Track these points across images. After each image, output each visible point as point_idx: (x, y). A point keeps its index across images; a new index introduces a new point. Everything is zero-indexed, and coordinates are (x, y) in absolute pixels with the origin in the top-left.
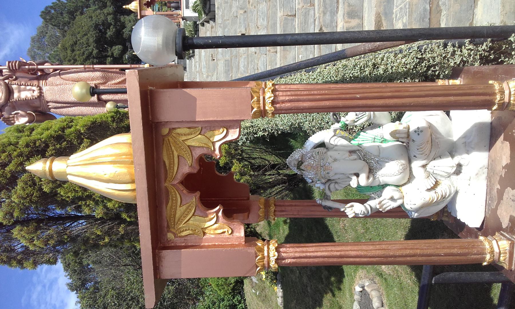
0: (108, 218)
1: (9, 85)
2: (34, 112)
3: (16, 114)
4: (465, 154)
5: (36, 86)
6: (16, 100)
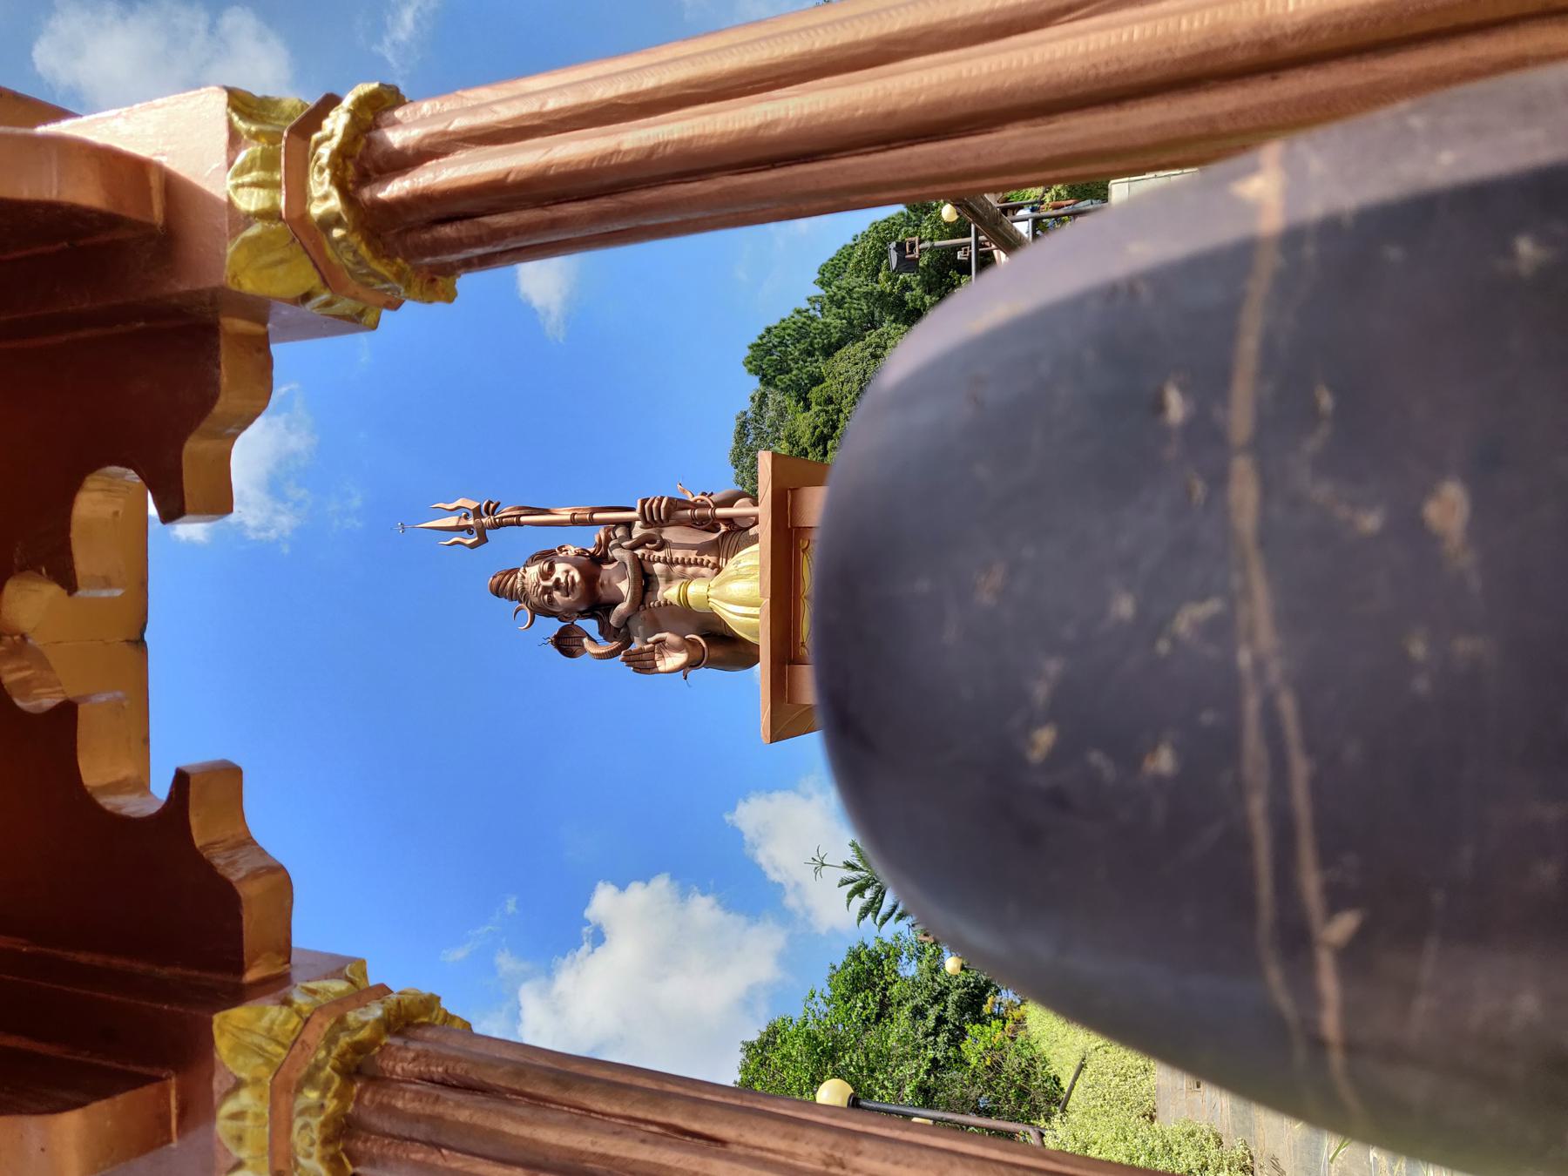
1: (645, 563)
2: (702, 637)
3: (657, 642)
5: (710, 565)
6: (659, 603)
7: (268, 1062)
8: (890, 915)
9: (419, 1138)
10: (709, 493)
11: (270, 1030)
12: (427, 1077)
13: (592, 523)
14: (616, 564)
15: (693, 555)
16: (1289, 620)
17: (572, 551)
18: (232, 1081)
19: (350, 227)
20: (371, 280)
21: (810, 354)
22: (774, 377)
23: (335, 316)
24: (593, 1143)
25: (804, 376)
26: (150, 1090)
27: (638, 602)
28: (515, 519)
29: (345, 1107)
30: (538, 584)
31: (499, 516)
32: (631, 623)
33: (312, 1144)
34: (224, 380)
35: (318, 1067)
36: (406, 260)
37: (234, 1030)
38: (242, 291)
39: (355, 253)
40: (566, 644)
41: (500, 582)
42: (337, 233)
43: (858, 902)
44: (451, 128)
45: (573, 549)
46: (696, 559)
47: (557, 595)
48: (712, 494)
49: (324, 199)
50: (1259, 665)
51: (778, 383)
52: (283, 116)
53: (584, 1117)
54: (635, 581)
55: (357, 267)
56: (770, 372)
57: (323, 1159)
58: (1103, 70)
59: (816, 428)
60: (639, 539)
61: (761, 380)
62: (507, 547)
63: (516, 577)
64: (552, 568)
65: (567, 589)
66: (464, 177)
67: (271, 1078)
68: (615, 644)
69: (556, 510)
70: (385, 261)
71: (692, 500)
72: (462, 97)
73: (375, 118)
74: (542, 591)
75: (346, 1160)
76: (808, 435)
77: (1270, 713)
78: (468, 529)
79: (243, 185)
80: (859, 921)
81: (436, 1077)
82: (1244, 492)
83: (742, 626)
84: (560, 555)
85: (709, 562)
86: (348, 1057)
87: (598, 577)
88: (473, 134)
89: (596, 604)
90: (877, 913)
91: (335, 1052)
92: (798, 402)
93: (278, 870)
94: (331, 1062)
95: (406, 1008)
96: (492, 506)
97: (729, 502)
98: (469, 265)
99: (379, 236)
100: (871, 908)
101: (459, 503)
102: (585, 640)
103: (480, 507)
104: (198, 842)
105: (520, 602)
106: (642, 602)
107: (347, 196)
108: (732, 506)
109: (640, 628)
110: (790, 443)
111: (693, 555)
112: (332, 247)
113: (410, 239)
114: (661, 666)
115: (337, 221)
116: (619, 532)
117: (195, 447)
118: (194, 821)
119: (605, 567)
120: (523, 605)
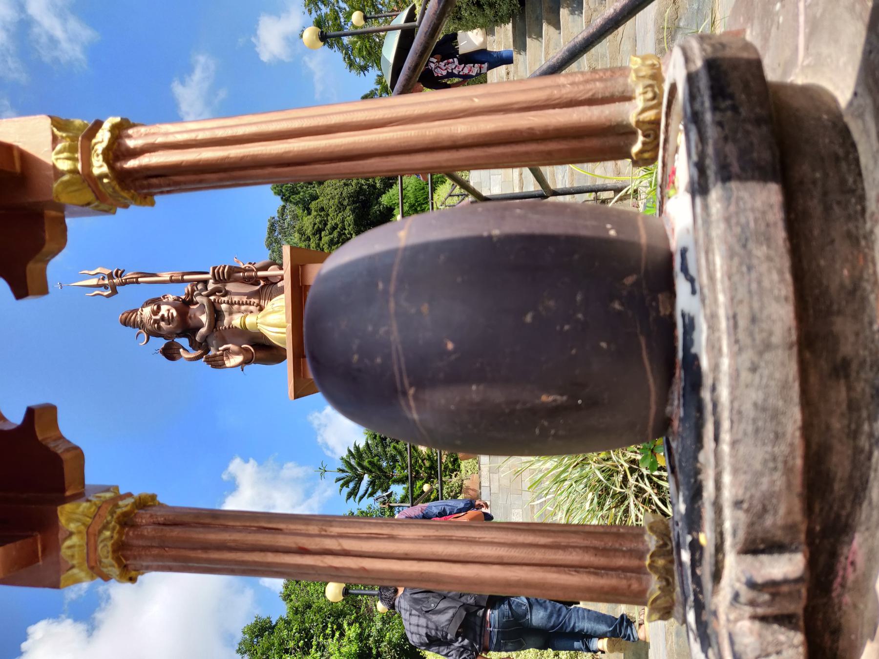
0: (127, 529)
1: (216, 304)
2: (252, 346)
4: (126, 582)
7: (84, 524)
8: (364, 495)
10: (253, 263)
11: (83, 512)
13: (183, 281)
14: (198, 305)
15: (244, 299)
17: (171, 298)
18: (68, 533)
20: (120, 199)
22: (290, 197)
25: (307, 195)
26: (30, 540)
27: (212, 326)
28: (135, 280)
30: (151, 318)
31: (124, 278)
32: (209, 340)
33: (108, 552)
34: (47, 237)
35: (108, 523)
36: (135, 191)
39: (113, 188)
40: (170, 353)
41: (126, 318)
42: (105, 181)
43: (346, 490)
45: (172, 297)
46: (247, 301)
47: (162, 324)
48: (255, 263)
49: (99, 167)
51: (292, 200)
53: (226, 528)
56: (287, 194)
57: (113, 558)
58: (403, 145)
59: (315, 224)
60: (212, 290)
61: (282, 198)
62: (128, 297)
63: (137, 314)
64: (159, 308)
65: (169, 320)
68: (199, 352)
69: (158, 274)
71: (243, 267)
74: (153, 322)
76: (310, 228)
77: (397, 351)
78: (105, 287)
79: (60, 159)
80: (347, 500)
81: (161, 522)
82: (392, 305)
83: (276, 339)
84: (164, 301)
85: (254, 302)
87: (188, 313)
89: (187, 328)
90: (356, 495)
91: (115, 516)
92: (304, 210)
93: (77, 448)
94: (114, 520)
96: (119, 272)
97: (265, 268)
98: (162, 193)
100: (353, 493)
101: (98, 270)
102: (181, 350)
103: (112, 272)
104: (40, 438)
105: (140, 329)
106: (215, 327)
107: (111, 166)
108: (267, 270)
109: (214, 342)
110: (300, 234)
111: (244, 299)
113: (137, 183)
114: (228, 363)
115: (106, 176)
116: (200, 287)
117: (32, 267)
118: (37, 429)
119: (192, 307)
120: (142, 331)
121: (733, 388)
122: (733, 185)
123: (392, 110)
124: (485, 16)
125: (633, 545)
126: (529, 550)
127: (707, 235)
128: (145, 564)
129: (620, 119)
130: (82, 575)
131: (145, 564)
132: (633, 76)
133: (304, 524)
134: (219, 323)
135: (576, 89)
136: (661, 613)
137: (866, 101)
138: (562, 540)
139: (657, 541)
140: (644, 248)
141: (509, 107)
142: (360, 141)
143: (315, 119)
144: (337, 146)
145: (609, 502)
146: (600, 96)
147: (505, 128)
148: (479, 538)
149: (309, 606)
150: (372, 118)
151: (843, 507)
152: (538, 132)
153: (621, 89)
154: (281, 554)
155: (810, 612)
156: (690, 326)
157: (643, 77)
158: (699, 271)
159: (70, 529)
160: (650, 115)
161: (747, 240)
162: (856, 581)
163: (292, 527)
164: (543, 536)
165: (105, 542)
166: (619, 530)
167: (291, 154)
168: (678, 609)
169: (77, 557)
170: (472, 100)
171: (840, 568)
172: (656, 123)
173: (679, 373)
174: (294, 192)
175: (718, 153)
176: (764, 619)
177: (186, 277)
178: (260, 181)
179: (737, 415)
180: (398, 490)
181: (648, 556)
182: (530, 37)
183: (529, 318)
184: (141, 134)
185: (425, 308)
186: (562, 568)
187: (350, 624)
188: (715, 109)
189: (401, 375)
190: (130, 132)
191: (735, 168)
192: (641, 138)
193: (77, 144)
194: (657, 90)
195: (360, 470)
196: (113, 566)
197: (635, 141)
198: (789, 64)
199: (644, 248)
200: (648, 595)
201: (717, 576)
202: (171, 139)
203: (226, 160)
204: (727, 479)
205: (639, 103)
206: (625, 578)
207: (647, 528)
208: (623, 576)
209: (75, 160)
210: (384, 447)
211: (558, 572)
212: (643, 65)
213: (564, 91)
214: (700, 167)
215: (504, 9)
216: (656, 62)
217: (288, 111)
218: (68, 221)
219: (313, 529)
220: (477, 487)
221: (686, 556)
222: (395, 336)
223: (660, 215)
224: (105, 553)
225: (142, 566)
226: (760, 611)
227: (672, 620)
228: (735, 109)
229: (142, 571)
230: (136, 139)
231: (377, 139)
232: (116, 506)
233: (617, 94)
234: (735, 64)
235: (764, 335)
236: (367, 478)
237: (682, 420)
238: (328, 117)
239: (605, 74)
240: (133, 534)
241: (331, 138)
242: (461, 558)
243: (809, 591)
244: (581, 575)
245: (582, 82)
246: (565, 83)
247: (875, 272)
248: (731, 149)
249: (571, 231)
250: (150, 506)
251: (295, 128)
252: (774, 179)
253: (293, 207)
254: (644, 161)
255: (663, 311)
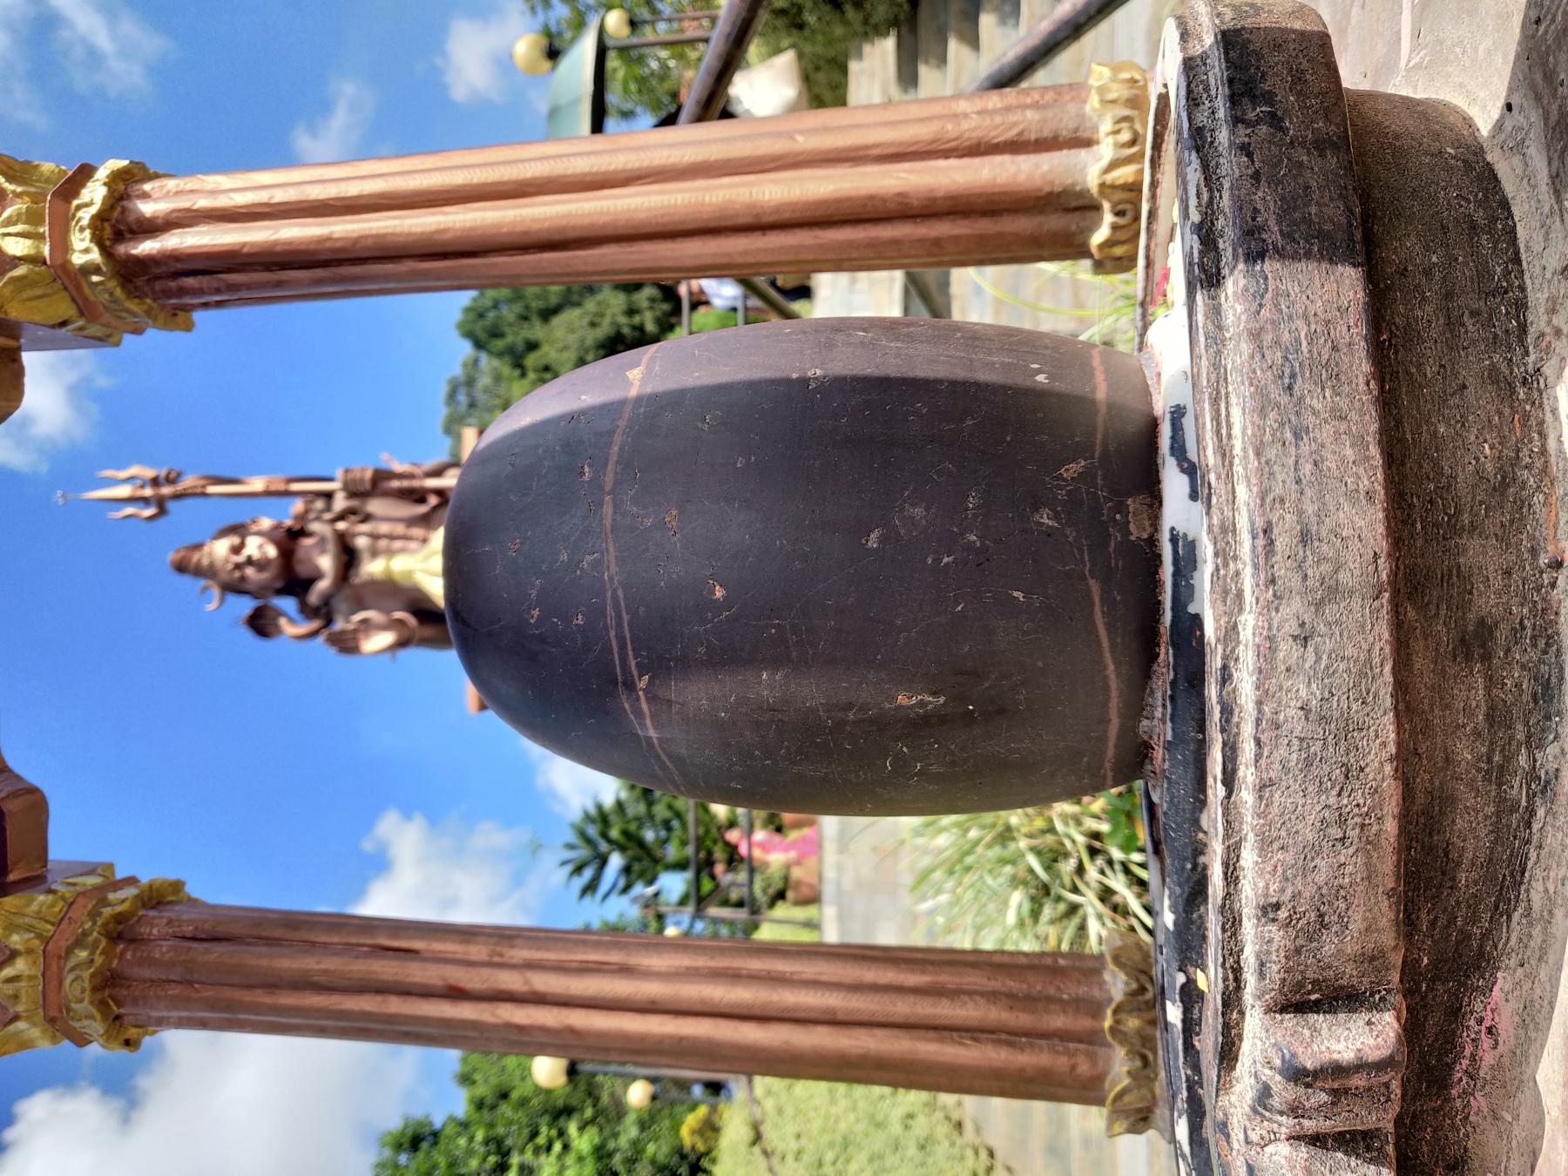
0: (122, 946)
7: (39, 936)
9: (176, 979)
11: (39, 912)
12: (180, 935)
13: (288, 494)
16: (621, 561)
17: (266, 523)
18: (8, 952)
19: (109, 275)
20: (124, 314)
21: (525, 318)
23: (86, 337)
24: (318, 963)
29: (111, 962)
33: (83, 991)
35: (85, 934)
36: (155, 300)
37: (7, 914)
38: (8, 318)
39: (111, 294)
40: (261, 623)
42: (95, 278)
44: (196, 207)
49: (83, 250)
50: (611, 579)
52: (43, 179)
53: (312, 946)
54: (337, 558)
55: (112, 305)
57: (92, 1002)
58: (660, 220)
65: (261, 565)
66: (205, 246)
67: (42, 948)
70: (136, 301)
72: (203, 181)
73: (126, 189)
75: (112, 1003)
77: (615, 597)
78: (145, 501)
81: (188, 935)
82: (608, 509)
86: (111, 926)
88: (214, 213)
89: (294, 581)
91: (100, 922)
93: (33, 791)
94: (97, 929)
95: (158, 890)
97: (438, 472)
98: (206, 305)
99: (131, 281)
101: (134, 470)
111: (400, 529)
112: (90, 287)
113: (158, 285)
115: (97, 270)
120: (210, 583)
121: (1262, 675)
122: (1269, 266)
123: (642, 155)
124: (846, 23)
125: (1082, 990)
126: (886, 997)
127: (1216, 366)
128: (155, 1014)
129: (1069, 181)
130: (35, 1032)
131: (155, 1014)
132: (1094, 101)
133: (461, 942)
134: (352, 572)
135: (988, 121)
136: (1132, 1119)
137: (1530, 118)
138: (947, 978)
139: (1127, 984)
140: (1103, 409)
141: (861, 153)
142: (580, 212)
143: (495, 168)
144: (535, 220)
145: (1048, 911)
146: (1033, 137)
147: (854, 193)
148: (792, 973)
149: (504, 1096)
150: (603, 168)
151: (1474, 919)
152: (915, 203)
153: (1072, 125)
154: (414, 998)
155: (1407, 1126)
156: (1187, 561)
157: (1113, 102)
158: (1200, 447)
159: (12, 946)
160: (1125, 174)
161: (1293, 376)
162: (1497, 1067)
163: (438, 946)
164: (913, 971)
165: (77, 972)
166: (1057, 962)
167: (448, 236)
168: (1161, 1112)
169: (24, 998)
170: (795, 140)
171: (1466, 1038)
172: (1134, 188)
173: (1166, 653)
174: (496, 333)
175: (1239, 204)
176: (1316, 1140)
177: (296, 487)
178: (391, 285)
179: (1269, 725)
180: (673, 884)
181: (1109, 1012)
182: (927, 62)
183: (873, 541)
184: (168, 192)
185: (672, 517)
186: (946, 1034)
187: (582, 1128)
188: (1236, 120)
189: (623, 647)
190: (147, 187)
191: (1273, 235)
192: (1108, 218)
193: (44, 207)
194: (1138, 127)
195: (604, 846)
196: (91, 1017)
197: (1096, 224)
198: (1388, 66)
199: (1103, 409)
200: (1107, 1085)
201: (1228, 1054)
202: (222, 202)
203: (328, 245)
204: (1248, 857)
205: (1106, 150)
206: (1064, 1054)
207: (1108, 958)
208: (1061, 1049)
209: (39, 237)
210: (650, 804)
211: (941, 1040)
212: (1114, 79)
213: (965, 125)
214: (1206, 235)
215: (881, 12)
216: (1137, 76)
217: (445, 154)
218: (27, 358)
219: (478, 951)
220: (814, 881)
221: (1174, 1013)
222: (612, 571)
223: (1140, 350)
224: (78, 993)
225: (150, 1017)
226: (1310, 1125)
227: (1151, 1133)
228: (1275, 121)
229: (150, 1029)
230: (156, 200)
231: (612, 209)
232: (104, 902)
233: (1064, 133)
234: (1279, 39)
235: (1326, 568)
236: (616, 861)
237: (1169, 746)
238: (520, 165)
239: (1042, 96)
240: (133, 956)
241: (526, 206)
242: (757, 1012)
243: (1404, 1085)
244: (983, 1047)
245: (1001, 109)
246: (969, 110)
247: (1544, 451)
248: (1265, 199)
249: (961, 374)
250: (171, 903)
251: (459, 186)
252: (1349, 258)
253: (496, 363)
254: (1114, 261)
255: (1137, 532)
